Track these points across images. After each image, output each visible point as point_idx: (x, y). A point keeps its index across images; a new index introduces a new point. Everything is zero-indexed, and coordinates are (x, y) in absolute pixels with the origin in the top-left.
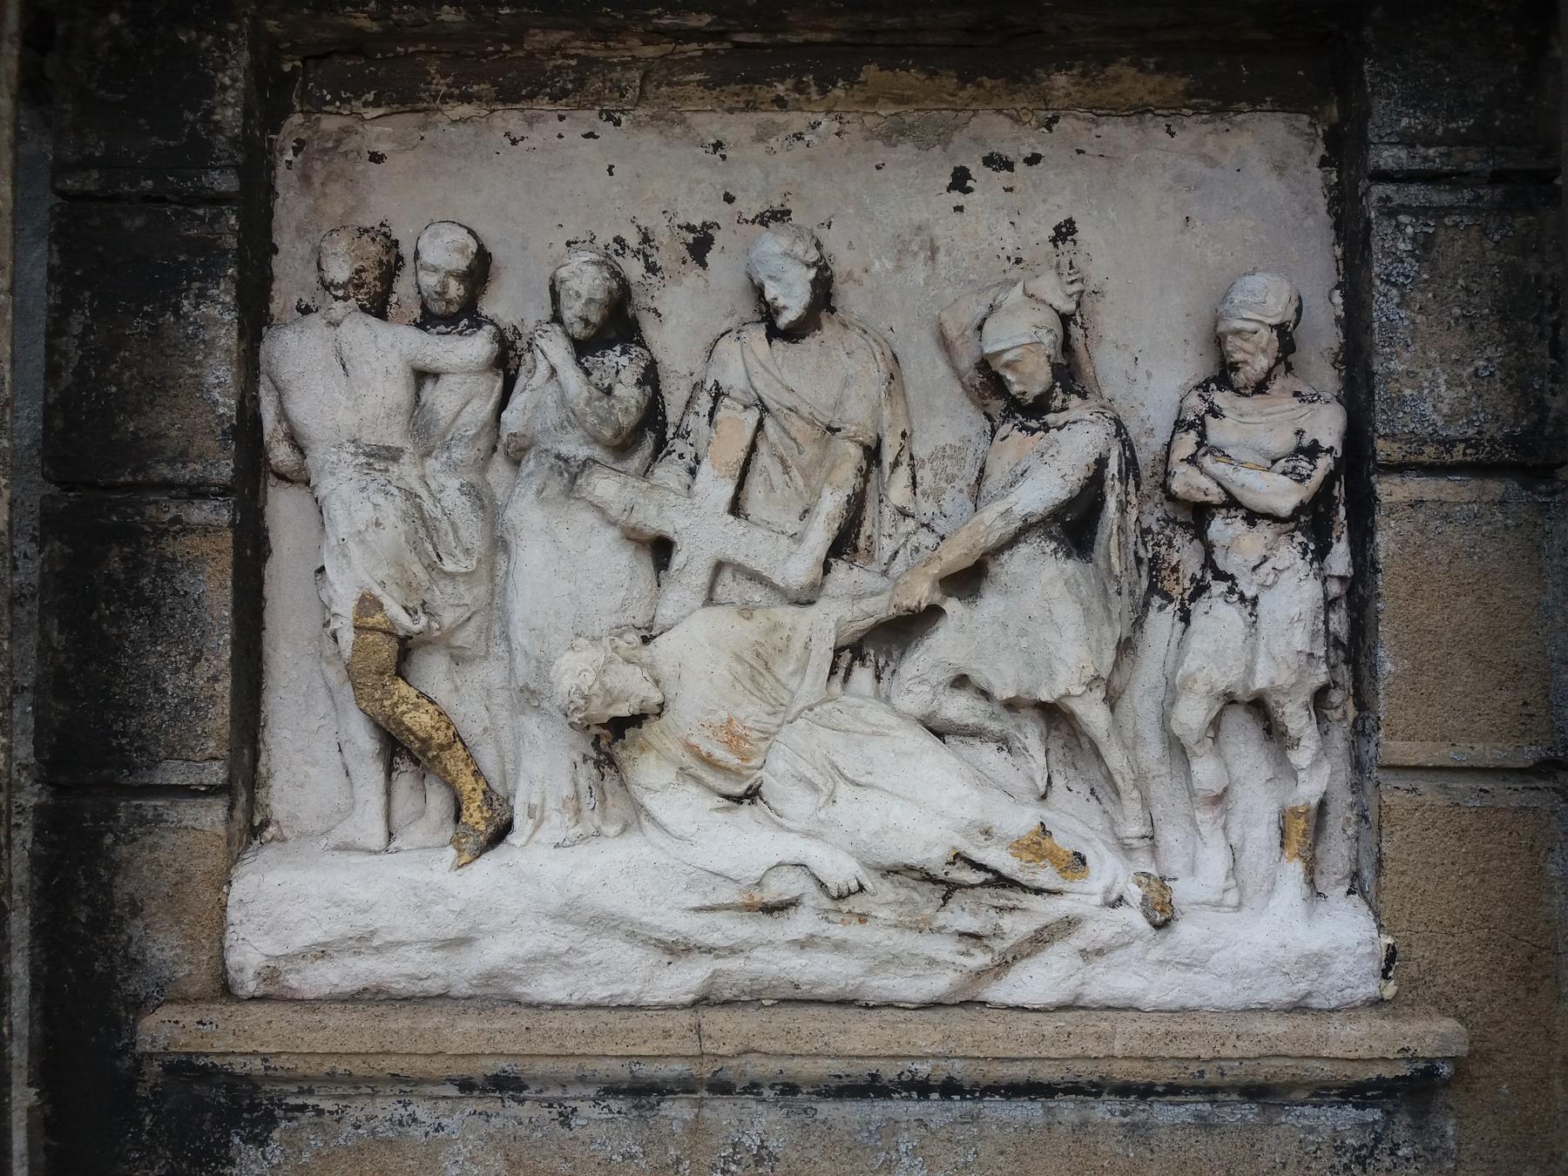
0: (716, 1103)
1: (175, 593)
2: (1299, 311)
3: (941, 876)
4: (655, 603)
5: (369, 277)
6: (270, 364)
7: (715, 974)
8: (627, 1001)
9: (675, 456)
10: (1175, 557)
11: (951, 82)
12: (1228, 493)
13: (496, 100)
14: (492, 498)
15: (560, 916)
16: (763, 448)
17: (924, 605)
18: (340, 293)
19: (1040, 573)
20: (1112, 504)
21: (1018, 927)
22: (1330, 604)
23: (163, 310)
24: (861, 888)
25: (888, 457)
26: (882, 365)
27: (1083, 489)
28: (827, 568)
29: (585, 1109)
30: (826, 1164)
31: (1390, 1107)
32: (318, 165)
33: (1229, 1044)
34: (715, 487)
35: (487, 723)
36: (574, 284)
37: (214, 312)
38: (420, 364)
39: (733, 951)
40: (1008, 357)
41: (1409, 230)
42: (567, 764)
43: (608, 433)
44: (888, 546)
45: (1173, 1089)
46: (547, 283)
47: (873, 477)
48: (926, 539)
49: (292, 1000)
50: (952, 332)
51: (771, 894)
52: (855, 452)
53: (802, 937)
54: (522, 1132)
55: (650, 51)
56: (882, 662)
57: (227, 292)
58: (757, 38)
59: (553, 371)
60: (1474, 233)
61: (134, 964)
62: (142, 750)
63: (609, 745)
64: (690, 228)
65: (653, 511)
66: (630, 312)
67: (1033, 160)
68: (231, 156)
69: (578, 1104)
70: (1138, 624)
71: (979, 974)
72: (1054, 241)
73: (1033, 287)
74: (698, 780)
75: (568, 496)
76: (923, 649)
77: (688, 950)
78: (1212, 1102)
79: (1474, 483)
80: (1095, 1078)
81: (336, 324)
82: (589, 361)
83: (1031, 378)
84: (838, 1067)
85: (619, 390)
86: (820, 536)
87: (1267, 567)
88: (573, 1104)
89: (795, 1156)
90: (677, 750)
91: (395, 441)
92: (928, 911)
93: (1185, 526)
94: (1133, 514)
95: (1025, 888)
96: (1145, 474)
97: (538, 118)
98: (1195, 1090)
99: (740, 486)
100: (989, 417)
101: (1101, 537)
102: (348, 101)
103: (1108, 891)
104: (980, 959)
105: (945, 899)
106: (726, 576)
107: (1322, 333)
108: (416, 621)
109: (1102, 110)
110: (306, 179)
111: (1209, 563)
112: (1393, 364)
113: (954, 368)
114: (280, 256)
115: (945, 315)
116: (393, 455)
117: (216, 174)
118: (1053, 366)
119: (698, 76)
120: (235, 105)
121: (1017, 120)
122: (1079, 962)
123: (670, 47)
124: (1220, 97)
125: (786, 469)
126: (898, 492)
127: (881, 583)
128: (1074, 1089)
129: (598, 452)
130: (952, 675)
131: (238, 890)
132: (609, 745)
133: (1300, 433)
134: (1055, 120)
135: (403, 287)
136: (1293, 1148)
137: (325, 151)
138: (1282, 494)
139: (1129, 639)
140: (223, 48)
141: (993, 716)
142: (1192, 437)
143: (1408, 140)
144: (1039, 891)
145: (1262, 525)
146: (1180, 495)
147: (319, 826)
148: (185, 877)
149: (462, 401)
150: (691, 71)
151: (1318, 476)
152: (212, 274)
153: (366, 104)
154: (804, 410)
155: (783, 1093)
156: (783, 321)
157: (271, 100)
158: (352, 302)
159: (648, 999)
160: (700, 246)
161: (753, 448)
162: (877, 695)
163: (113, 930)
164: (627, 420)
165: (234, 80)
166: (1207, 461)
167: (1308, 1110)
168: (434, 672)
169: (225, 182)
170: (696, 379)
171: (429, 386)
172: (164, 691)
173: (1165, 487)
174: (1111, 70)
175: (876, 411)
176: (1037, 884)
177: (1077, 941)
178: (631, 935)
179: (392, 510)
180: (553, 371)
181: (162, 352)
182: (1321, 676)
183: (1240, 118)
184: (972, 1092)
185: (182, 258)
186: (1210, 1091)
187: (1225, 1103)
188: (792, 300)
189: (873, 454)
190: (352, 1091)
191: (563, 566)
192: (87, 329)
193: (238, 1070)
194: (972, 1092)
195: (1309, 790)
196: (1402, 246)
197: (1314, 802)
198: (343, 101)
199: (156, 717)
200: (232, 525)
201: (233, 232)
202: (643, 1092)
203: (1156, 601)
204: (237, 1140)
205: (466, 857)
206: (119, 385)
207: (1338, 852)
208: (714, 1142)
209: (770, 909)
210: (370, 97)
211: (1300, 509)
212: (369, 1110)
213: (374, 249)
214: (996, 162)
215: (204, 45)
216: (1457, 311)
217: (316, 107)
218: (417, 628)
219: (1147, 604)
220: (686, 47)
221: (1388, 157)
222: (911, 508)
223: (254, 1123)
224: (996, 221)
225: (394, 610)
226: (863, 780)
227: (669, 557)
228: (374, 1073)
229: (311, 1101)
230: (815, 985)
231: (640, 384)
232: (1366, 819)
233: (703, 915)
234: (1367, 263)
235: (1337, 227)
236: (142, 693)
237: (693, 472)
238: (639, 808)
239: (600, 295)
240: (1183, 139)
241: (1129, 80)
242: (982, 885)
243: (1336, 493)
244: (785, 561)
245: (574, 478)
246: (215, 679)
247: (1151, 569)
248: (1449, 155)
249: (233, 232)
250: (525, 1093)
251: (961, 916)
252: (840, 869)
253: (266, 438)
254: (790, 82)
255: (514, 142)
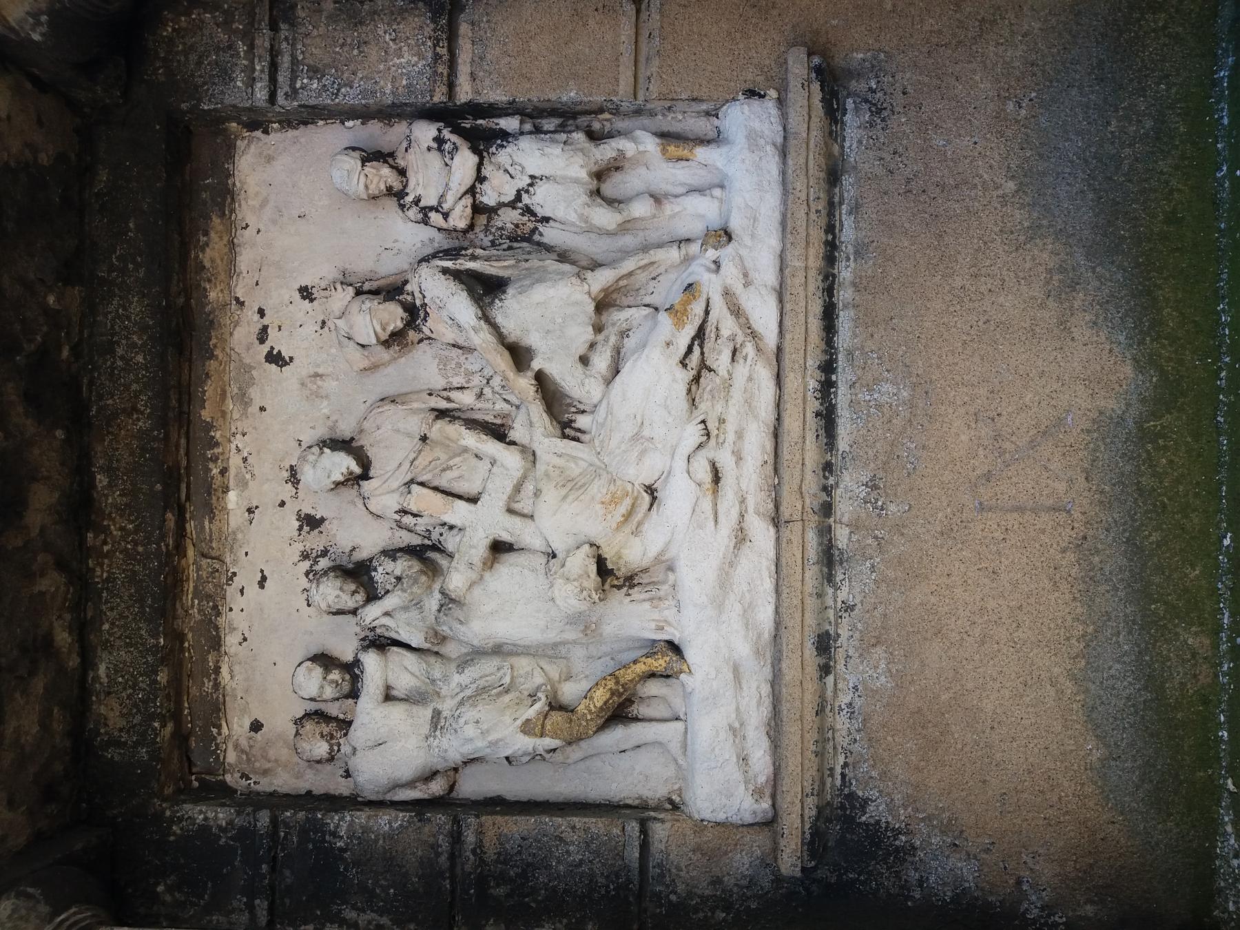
0: (838, 513)
1: (519, 853)
2: (354, 149)
3: (694, 372)
4: (535, 552)
5: (326, 730)
6: (378, 792)
7: (758, 513)
8: (773, 568)
9: (441, 539)
10: (509, 226)
11: (212, 365)
12: (465, 193)
13: (218, 650)
14: (467, 654)
15: (720, 607)
16: (435, 483)
17: (533, 382)
18: (336, 748)
19: (515, 312)
20: (471, 265)
21: (729, 326)
22: (538, 130)
23: (343, 859)
24: (703, 422)
25: (444, 405)
26: (386, 408)
27: (462, 282)
28: (513, 443)
29: (843, 595)
30: (878, 445)
31: (845, 93)
32: (257, 765)
33: (799, 195)
34: (458, 512)
35: (608, 658)
36: (331, 599)
37: (344, 826)
38: (381, 698)
39: (743, 501)
40: (378, 329)
41: (305, 81)
42: (633, 606)
43: (424, 578)
44: (501, 406)
45: (830, 229)
46: (331, 617)
47: (456, 414)
48: (496, 382)
49: (775, 780)
50: (366, 364)
51: (707, 477)
52: (440, 424)
53: (734, 459)
54: (857, 635)
55: (191, 552)
56: (573, 410)
57: (332, 819)
58: (183, 486)
59: (387, 614)
60: (308, 41)
61: (752, 882)
62: (617, 876)
63: (617, 578)
64: (300, 529)
65: (473, 551)
66: (351, 566)
67: (261, 312)
68: (248, 814)
69: (839, 600)
70: (549, 249)
71: (759, 350)
72: (312, 300)
73: (337, 314)
74: (640, 524)
75: (464, 605)
76: (563, 384)
77: (741, 529)
78: (841, 203)
79: (461, 41)
80: (821, 278)
81: (355, 749)
82: (381, 591)
83: (393, 315)
84: (810, 437)
85: (398, 572)
86: (491, 447)
87: (510, 169)
88: (839, 603)
89: (872, 465)
90: (620, 537)
91: (428, 713)
92: (718, 380)
93: (489, 219)
94: (479, 252)
95: (704, 321)
96: (456, 243)
97: (230, 624)
98: (831, 214)
99: (460, 497)
100: (421, 341)
101: (501, 273)
102: (217, 745)
103: (709, 270)
104: (749, 349)
105: (710, 370)
106: (517, 506)
107: (374, 133)
108: (540, 699)
109: (231, 269)
110: (265, 772)
111: (512, 205)
112: (387, 92)
113: (390, 362)
114: (313, 789)
115: (355, 368)
116: (437, 714)
117: (259, 824)
118: (385, 301)
119: (207, 523)
120: (217, 812)
121: (237, 324)
122: (752, 288)
123: (188, 541)
124: (225, 196)
125: (450, 468)
126: (465, 399)
127: (523, 410)
128: (829, 291)
129: (437, 586)
130: (579, 365)
131: (707, 815)
132: (617, 578)
133: (429, 149)
134: (237, 299)
135: (333, 710)
136: (871, 153)
137: (248, 760)
138: (465, 161)
139: (559, 255)
140: (181, 819)
141: (606, 340)
142: (433, 215)
143: (251, 82)
144: (707, 312)
145: (484, 172)
146: (468, 222)
147: (672, 767)
148: (697, 849)
149: (403, 671)
150: (203, 527)
151: (454, 138)
152: (320, 827)
153: (219, 734)
154: (412, 456)
155: (831, 472)
156: (357, 470)
157: (219, 792)
158: (341, 741)
159: (772, 554)
160: (311, 522)
161: (436, 489)
162: (593, 412)
163: (731, 896)
164: (416, 566)
165: (201, 812)
166: (446, 206)
167: (847, 144)
168: (570, 691)
169: (264, 818)
170: (394, 525)
171: (394, 693)
172: (581, 860)
173: (465, 232)
174: (207, 264)
175: (414, 412)
176: (702, 314)
177: (738, 288)
178: (731, 564)
179: (469, 714)
180: (387, 614)
181: (369, 860)
182: (579, 137)
183: (237, 184)
184: (831, 355)
185: (311, 846)
186: (831, 206)
187: (842, 197)
188: (344, 463)
189: (441, 414)
190: (831, 743)
191: (513, 607)
192: (354, 907)
193: (814, 813)
194: (831, 355)
195: (650, 144)
196: (315, 86)
197: (657, 140)
198: (217, 748)
199: (597, 867)
200: (477, 816)
201: (295, 814)
202: (829, 558)
203: (536, 237)
204: (864, 818)
205: (685, 667)
206: (389, 887)
207: (697, 125)
208: (863, 515)
209: (717, 479)
210: (215, 731)
211: (475, 150)
212: (844, 733)
213: (309, 726)
214: (263, 335)
215: (179, 832)
216: (355, 52)
217: (221, 764)
218: (544, 699)
219: (539, 244)
220: (188, 531)
221: (261, 94)
222: (477, 390)
223: (853, 807)
224: (298, 334)
225: (531, 713)
226: (640, 421)
227: (505, 543)
228: (815, 726)
229: (838, 770)
230: (764, 451)
231: (394, 560)
232: (670, 108)
233: (719, 520)
234: (324, 108)
235: (306, 123)
236: (582, 875)
237: (451, 527)
238: (658, 560)
239: (338, 583)
240: (251, 219)
241: (212, 254)
242: (702, 347)
243: (468, 126)
244: (507, 469)
245: (452, 600)
246: (573, 828)
247: (517, 241)
248: (260, 57)
249: (295, 814)
250: (832, 632)
251: (721, 361)
252: (693, 433)
253: (426, 796)
254: (211, 465)
255: (245, 639)
